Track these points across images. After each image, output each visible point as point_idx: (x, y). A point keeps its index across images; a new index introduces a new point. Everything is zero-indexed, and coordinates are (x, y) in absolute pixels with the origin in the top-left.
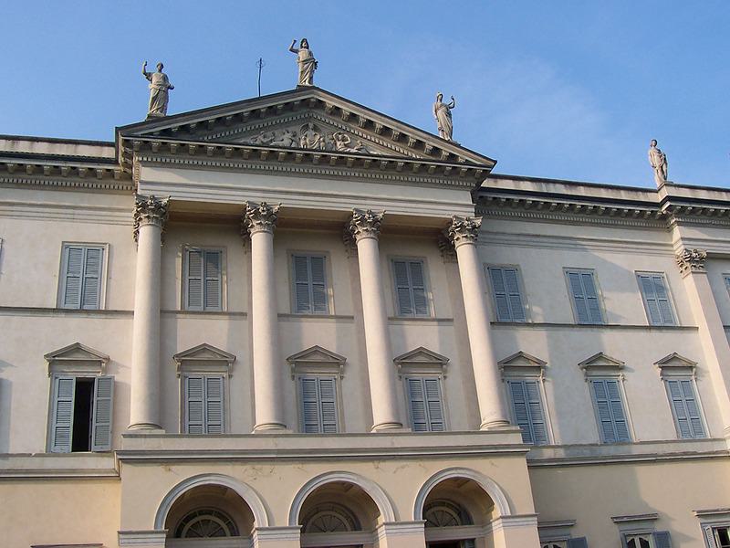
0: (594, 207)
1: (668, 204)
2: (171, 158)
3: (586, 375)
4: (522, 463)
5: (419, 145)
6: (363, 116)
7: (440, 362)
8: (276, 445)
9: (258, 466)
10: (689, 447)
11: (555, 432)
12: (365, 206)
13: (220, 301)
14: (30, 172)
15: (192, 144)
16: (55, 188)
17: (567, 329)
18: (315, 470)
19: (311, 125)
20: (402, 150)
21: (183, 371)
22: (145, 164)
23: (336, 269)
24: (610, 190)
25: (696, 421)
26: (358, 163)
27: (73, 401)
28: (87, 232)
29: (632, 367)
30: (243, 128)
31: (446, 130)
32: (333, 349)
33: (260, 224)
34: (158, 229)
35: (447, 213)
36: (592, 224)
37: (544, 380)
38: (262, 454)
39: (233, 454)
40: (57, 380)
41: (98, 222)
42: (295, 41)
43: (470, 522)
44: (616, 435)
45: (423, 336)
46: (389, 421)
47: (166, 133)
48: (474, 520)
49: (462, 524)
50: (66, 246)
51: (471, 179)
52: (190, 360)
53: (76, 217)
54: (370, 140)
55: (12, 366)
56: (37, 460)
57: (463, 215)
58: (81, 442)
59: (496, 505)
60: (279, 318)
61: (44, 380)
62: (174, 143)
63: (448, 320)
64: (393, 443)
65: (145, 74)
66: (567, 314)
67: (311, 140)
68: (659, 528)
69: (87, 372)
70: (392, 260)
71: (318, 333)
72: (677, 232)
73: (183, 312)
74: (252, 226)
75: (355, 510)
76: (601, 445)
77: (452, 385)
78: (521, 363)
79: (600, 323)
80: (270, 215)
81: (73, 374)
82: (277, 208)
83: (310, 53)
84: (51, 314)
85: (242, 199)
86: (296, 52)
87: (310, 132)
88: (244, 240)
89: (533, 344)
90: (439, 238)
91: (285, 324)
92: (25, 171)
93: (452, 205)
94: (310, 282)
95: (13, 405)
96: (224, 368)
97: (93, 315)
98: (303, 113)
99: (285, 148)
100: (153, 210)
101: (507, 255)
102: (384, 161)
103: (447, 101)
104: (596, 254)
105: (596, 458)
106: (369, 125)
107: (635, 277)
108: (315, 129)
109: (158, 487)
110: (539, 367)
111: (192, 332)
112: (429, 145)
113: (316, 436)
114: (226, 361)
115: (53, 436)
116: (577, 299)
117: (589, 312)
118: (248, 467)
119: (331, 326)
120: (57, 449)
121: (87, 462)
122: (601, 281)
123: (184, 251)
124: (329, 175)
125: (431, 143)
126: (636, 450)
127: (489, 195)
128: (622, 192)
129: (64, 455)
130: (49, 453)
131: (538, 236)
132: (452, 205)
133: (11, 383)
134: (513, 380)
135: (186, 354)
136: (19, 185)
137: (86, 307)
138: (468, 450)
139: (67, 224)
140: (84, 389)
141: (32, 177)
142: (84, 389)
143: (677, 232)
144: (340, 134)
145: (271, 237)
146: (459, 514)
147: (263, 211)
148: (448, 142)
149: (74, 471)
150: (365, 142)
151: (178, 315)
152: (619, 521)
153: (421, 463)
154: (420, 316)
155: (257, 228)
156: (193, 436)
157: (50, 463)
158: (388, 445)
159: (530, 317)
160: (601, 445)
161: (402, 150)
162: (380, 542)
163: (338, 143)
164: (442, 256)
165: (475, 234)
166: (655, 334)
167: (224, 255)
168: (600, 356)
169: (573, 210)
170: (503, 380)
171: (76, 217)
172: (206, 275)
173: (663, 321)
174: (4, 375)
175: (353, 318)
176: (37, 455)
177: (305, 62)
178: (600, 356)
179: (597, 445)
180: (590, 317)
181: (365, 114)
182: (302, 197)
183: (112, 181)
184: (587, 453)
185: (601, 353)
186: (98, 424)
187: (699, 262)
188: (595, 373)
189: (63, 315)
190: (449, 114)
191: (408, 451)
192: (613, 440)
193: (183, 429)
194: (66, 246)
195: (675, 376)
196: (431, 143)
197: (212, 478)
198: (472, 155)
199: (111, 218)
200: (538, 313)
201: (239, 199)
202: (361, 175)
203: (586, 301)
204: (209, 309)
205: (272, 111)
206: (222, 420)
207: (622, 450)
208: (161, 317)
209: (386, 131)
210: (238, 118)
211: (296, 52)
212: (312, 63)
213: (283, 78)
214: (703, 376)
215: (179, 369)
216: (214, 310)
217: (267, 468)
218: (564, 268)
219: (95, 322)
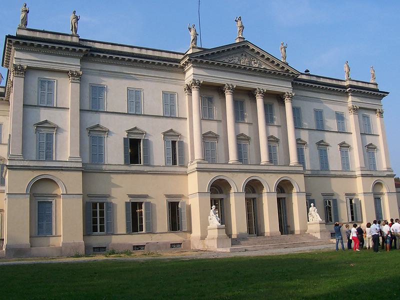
1: (349, 89)
4: (303, 176)
6: (262, 53)
7: (216, 137)
10: (345, 173)
15: (205, 61)
16: (157, 70)
18: (249, 175)
24: (55, 35)
25: (348, 164)
28: (170, 88)
29: (150, 134)
41: (172, 84)
43: (284, 192)
45: (245, 129)
48: (286, 192)
49: (253, 193)
59: (232, 188)
63: (220, 121)
66: (314, 126)
67: (244, 62)
68: (334, 198)
71: (369, 140)
72: (350, 99)
75: (254, 187)
77: (219, 146)
78: (344, 145)
81: (170, 139)
89: (305, 136)
90: (280, 98)
92: (26, 45)
93: (285, 87)
97: (174, 119)
101: (299, 104)
104: (326, 104)
107: (335, 114)
108: (245, 56)
115: (167, 160)
120: (168, 164)
121: (134, 167)
122: (325, 114)
126: (108, 168)
128: (49, 35)
131: (307, 97)
135: (92, 128)
143: (350, 99)
146: (281, 190)
152: (323, 195)
154: (242, 121)
157: (167, 169)
162: (263, 197)
165: (292, 98)
166: (339, 134)
168: (322, 141)
173: (342, 131)
175: (221, 121)
177: (241, 27)
178: (322, 141)
180: (321, 128)
184: (316, 173)
187: (356, 110)
188: (320, 146)
195: (370, 151)
204: (210, 118)
207: (326, 172)
210: (223, 51)
211: (237, 21)
214: (62, 133)
216: (211, 119)
217: (236, 174)
219: (175, 121)
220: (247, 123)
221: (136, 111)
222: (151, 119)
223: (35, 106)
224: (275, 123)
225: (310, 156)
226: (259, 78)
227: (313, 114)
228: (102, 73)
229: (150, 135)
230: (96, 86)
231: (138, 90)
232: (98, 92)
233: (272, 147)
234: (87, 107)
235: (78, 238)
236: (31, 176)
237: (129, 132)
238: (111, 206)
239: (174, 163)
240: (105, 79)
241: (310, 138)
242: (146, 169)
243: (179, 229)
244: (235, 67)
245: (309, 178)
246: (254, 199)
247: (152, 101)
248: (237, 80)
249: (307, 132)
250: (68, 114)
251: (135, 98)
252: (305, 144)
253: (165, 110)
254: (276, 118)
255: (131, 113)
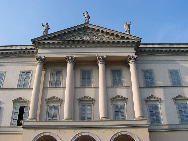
0: (178, 50)
2: (66, 46)
3: (175, 102)
4: (146, 130)
5: (118, 36)
8: (67, 124)
9: (61, 130)
11: (164, 120)
12: (100, 55)
13: (60, 83)
14: (14, 54)
15: (51, 42)
17: (169, 88)
18: (78, 131)
19: (86, 34)
20: (113, 38)
21: (147, 103)
22: (39, 48)
23: (124, 73)
26: (99, 42)
27: (18, 113)
28: (27, 68)
30: (66, 37)
31: (128, 31)
32: (126, 97)
33: (132, 61)
34: (104, 64)
35: (126, 55)
36: (178, 55)
37: (160, 104)
38: (33, 126)
39: (131, 125)
40: (15, 107)
41: (30, 65)
42: (84, 12)
44: (186, 121)
46: (103, 117)
47: (45, 39)
50: (21, 72)
51: (134, 44)
52: (113, 100)
53: (24, 64)
54: (103, 36)
55: (4, 103)
56: (8, 128)
57: (131, 55)
58: (19, 124)
60: (106, 88)
61: (12, 107)
62: (46, 42)
64: (103, 124)
65: (43, 26)
67: (86, 38)
69: (23, 105)
70: (112, 70)
73: (50, 88)
74: (130, 62)
76: (180, 124)
77: (126, 107)
78: (152, 99)
79: (148, 86)
80: (72, 59)
81: (19, 105)
82: (105, 57)
83: (88, 15)
84: (16, 90)
85: (65, 55)
86: (85, 15)
87: (86, 36)
88: (127, 66)
90: (125, 62)
91: (143, 90)
93: (129, 52)
94: (86, 78)
95: (4, 114)
96: (59, 103)
97: (26, 90)
98: (84, 31)
99: (112, 40)
100: (40, 60)
102: (106, 41)
103: (129, 23)
105: (177, 129)
106: (103, 32)
108: (87, 35)
110: (158, 100)
111: (51, 93)
112: (121, 35)
113: (86, 121)
114: (93, 101)
115: (12, 122)
116: (172, 78)
117: (176, 83)
118: (58, 130)
119: (125, 90)
120: (13, 126)
122: (181, 73)
123: (51, 71)
124: (90, 47)
125: (121, 35)
126: (163, 127)
127: (142, 49)
129: (14, 127)
130: (11, 127)
132: (129, 52)
133: (4, 108)
134: (149, 104)
135: (49, 99)
136: (11, 57)
137: (24, 88)
138: (127, 126)
139: (22, 66)
140: (22, 110)
141: (14, 55)
142: (22, 110)
144: (94, 35)
145: (104, 65)
147: (70, 58)
148: (128, 35)
149: (16, 131)
150: (102, 37)
151: (48, 89)
153: (112, 130)
155: (100, 63)
156: (49, 121)
157: (11, 129)
158: (102, 124)
159: (156, 85)
160: (180, 124)
161: (113, 38)
163: (94, 38)
164: (127, 68)
165: (135, 60)
167: (62, 72)
168: (180, 96)
169: (171, 52)
170: (175, 104)
171: (24, 64)
172: (57, 77)
174: (1, 106)
176: (8, 127)
177: (86, 17)
179: (178, 124)
181: (101, 29)
182: (82, 54)
183: (34, 54)
184: (175, 127)
185: (180, 95)
186: (49, 118)
188: (178, 101)
189: (18, 90)
190: (129, 27)
191: (107, 126)
192: (184, 123)
193: (46, 120)
194: (21, 72)
196: (121, 35)
197: (48, 133)
198: (134, 37)
199: (34, 64)
200: (159, 83)
201: (64, 55)
202: (100, 46)
203: (176, 80)
205: (74, 31)
206: (57, 118)
208: (107, 89)
209: (107, 33)
211: (85, 15)
212: (89, 18)
213: (81, 21)
215: (47, 103)
217: (64, 131)
218: (168, 69)
220: (93, 87)
221: (56, 85)
222: (7, 91)
223: (143, 87)
224: (124, 85)
225: (166, 110)
226: (100, 49)
227: (168, 74)
229: (3, 103)
230: (172, 70)
231: (176, 70)
233: (119, 106)
239: (19, 124)
240: (152, 65)
241: (165, 94)
244: (88, 43)
245: (166, 133)
248: (78, 53)
249: (161, 90)
252: (158, 100)
254: (125, 80)
255: (52, 87)
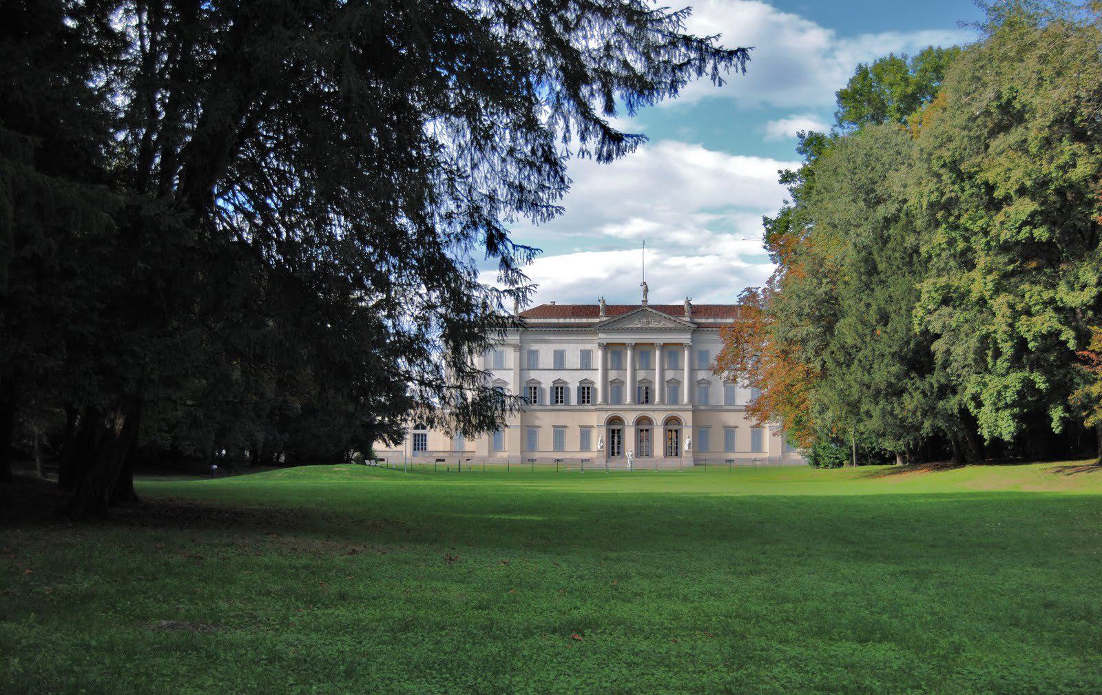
18: (668, 413)
109: (605, 416)
132: (685, 338)
157: (578, 407)
228: (536, 341)
232: (534, 355)
234: (525, 367)
235: (517, 453)
236: (610, 414)
237: (554, 382)
238: (568, 389)
242: (567, 408)
243: (535, 402)
246: (619, 431)
247: (573, 359)
250: (511, 373)
251: (559, 358)
253: (582, 364)
